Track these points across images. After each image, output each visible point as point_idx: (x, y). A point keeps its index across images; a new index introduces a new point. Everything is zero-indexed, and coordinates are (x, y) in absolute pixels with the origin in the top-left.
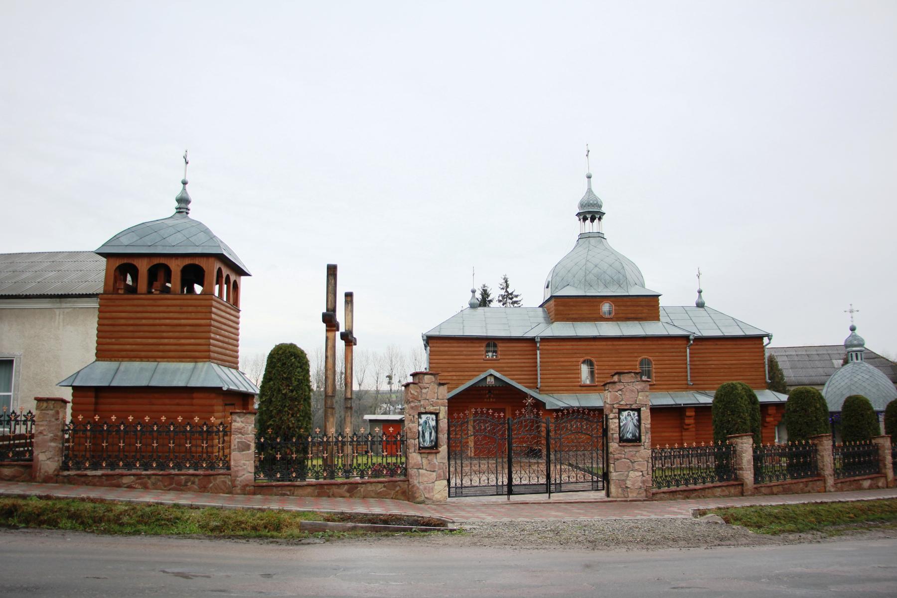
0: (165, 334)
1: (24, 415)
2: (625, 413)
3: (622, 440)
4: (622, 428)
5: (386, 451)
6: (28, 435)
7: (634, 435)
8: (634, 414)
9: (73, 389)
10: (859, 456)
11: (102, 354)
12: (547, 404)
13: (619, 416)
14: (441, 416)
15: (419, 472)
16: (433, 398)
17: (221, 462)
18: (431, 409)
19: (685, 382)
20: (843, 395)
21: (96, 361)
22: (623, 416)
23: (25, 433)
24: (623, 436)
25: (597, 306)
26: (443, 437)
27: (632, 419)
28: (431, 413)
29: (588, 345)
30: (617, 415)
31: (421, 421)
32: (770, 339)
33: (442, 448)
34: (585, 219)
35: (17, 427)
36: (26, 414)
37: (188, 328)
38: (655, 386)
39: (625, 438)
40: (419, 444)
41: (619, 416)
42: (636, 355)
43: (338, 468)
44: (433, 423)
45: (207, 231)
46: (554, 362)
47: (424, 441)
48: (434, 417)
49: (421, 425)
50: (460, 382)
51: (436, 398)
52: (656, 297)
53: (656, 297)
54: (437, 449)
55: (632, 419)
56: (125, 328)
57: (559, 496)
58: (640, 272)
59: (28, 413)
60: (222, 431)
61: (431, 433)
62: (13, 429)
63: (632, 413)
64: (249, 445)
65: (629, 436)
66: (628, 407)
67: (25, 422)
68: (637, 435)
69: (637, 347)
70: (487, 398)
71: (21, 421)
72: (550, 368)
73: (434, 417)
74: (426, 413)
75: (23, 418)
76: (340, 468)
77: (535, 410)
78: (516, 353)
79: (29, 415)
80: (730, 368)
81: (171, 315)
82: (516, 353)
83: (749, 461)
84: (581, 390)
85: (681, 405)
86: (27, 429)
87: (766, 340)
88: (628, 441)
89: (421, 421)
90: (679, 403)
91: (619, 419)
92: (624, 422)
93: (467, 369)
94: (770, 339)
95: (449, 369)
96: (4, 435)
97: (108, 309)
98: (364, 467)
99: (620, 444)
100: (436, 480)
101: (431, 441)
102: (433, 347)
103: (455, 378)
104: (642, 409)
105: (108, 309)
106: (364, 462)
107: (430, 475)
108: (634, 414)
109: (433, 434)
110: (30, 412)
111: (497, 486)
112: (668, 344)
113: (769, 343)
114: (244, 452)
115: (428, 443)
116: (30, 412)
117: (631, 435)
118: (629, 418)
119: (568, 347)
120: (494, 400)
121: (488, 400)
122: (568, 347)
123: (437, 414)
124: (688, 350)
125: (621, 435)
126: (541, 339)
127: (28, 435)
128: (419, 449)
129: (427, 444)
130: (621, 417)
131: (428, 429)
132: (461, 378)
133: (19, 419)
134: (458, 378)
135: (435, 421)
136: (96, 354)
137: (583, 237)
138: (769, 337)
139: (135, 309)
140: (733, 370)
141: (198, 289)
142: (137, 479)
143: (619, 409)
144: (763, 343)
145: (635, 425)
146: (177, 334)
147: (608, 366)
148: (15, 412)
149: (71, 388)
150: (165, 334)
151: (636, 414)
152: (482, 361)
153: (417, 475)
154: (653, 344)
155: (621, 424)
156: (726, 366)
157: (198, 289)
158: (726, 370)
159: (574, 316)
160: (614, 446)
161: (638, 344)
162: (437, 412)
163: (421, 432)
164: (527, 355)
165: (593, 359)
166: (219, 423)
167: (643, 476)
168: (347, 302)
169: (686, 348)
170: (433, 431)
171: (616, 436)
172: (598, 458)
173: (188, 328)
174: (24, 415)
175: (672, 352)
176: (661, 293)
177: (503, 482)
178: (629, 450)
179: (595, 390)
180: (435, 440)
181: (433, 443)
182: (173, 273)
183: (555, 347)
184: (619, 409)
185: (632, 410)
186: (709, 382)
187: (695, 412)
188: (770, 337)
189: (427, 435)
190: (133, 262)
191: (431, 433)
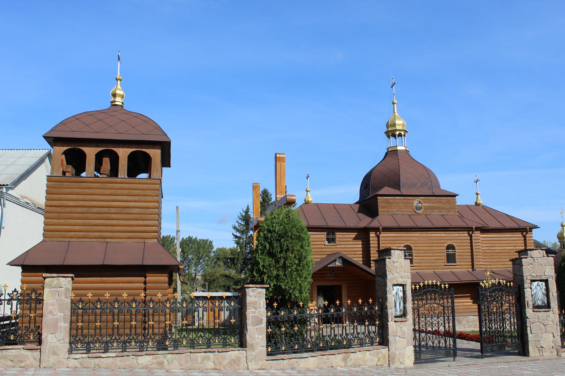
0: (113, 216)
1: (8, 294)
2: (535, 284)
4: (534, 296)
6: (13, 316)
7: (543, 302)
8: (542, 284)
9: (22, 269)
15: (395, 339)
16: (402, 272)
17: (201, 338)
20: (248, 296)
22: (533, 286)
23: (10, 314)
26: (409, 305)
27: (541, 289)
33: (409, 315)
37: (137, 210)
39: (536, 304)
42: (443, 241)
43: (30, 330)
44: (401, 294)
45: (159, 128)
48: (401, 288)
51: (403, 271)
55: (541, 289)
59: (13, 292)
60: (81, 309)
63: (540, 283)
64: (262, 320)
65: (539, 303)
68: (546, 302)
70: (328, 277)
71: (5, 300)
75: (8, 297)
79: (15, 293)
81: (119, 198)
86: (11, 309)
88: (539, 307)
92: (535, 291)
96: (4, 315)
97: (56, 190)
100: (407, 346)
101: (401, 311)
104: (549, 280)
105: (56, 190)
106: (362, 331)
108: (542, 284)
110: (15, 290)
116: (15, 290)
117: (541, 302)
118: (538, 288)
120: (333, 278)
121: (329, 279)
127: (13, 316)
130: (532, 286)
131: (398, 300)
135: (402, 293)
142: (152, 359)
145: (543, 294)
149: (20, 268)
150: (113, 216)
151: (544, 283)
152: (323, 246)
153: (394, 342)
156: (506, 251)
158: (506, 254)
160: (529, 312)
166: (166, 299)
167: (554, 337)
170: (401, 301)
171: (531, 303)
173: (137, 210)
174: (8, 294)
176: (458, 193)
178: (542, 314)
180: (403, 309)
181: (402, 312)
182: (120, 158)
185: (541, 281)
186: (495, 263)
190: (113, 149)
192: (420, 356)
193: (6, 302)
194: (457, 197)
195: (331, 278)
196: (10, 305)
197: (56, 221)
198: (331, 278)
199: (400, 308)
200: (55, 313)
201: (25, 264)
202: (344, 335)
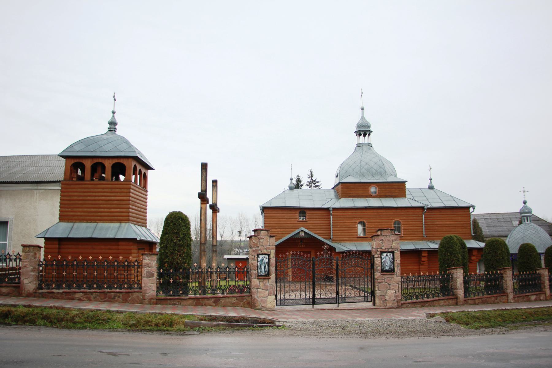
0: (101, 206)
1: (15, 256)
2: (385, 254)
3: (383, 271)
4: (383, 264)
5: (238, 278)
6: (17, 268)
7: (390, 268)
8: (390, 255)
9: (45, 239)
10: (529, 280)
11: (63, 218)
12: (336, 249)
13: (381, 256)
14: (271, 256)
15: (258, 290)
16: (267, 245)
17: (136, 284)
18: (265, 252)
19: (421, 235)
21: (59, 222)
22: (383, 256)
23: (15, 266)
24: (384, 268)
25: (367, 188)
26: (273, 269)
27: (389, 258)
28: (265, 254)
29: (362, 212)
30: (380, 255)
31: (259, 259)
32: (474, 209)
33: (272, 275)
34: (360, 135)
35: (11, 263)
36: (16, 255)
38: (403, 238)
39: (385, 269)
40: (258, 273)
41: (381, 256)
42: (391, 218)
44: (267, 261)
46: (341, 223)
47: (261, 272)
48: (267, 256)
49: (259, 261)
50: (283, 235)
51: (268, 245)
52: (404, 183)
53: (404, 183)
54: (269, 276)
55: (389, 258)
56: (77, 202)
57: (344, 305)
58: (394, 168)
59: (17, 254)
60: (136, 265)
61: (265, 267)
62: (8, 264)
63: (389, 254)
64: (153, 274)
65: (387, 268)
66: (387, 250)
67: (15, 260)
68: (392, 267)
69: (392, 213)
70: (300, 245)
71: (13, 259)
72: (338, 226)
73: (267, 256)
74: (262, 254)
75: (14, 257)
76: (209, 288)
77: (329, 253)
78: (317, 217)
79: (18, 255)
80: (449, 227)
81: (105, 194)
82: (317, 217)
83: (461, 284)
84: (358, 240)
85: (419, 249)
86: (16, 264)
87: (471, 209)
88: (386, 271)
89: (259, 259)
90: (418, 248)
91: (381, 258)
92: (384, 260)
93: (287, 227)
94: (474, 209)
95: (276, 227)
98: (224, 288)
99: (382, 273)
100: (268, 296)
101: (265, 272)
102: (267, 213)
103: (280, 232)
104: (395, 252)
107: (265, 292)
108: (390, 255)
109: (267, 267)
110: (18, 254)
111: (306, 299)
112: (411, 212)
113: (473, 211)
114: (150, 278)
115: (264, 273)
116: (18, 254)
117: (388, 268)
118: (387, 257)
119: (350, 214)
120: (304, 246)
122: (350, 214)
123: (269, 255)
124: (423, 216)
125: (382, 268)
126: (333, 208)
127: (17, 268)
128: (258, 277)
129: (263, 273)
130: (382, 256)
131: (263, 264)
132: (284, 232)
133: (12, 258)
134: (282, 232)
136: (59, 218)
137: (359, 146)
138: (473, 207)
139: (83, 190)
140: (451, 228)
141: (122, 178)
143: (381, 252)
144: (469, 211)
145: (391, 262)
146: (109, 206)
147: (374, 225)
148: (10, 253)
150: (101, 206)
151: (391, 255)
152: (297, 222)
153: (257, 292)
154: (402, 212)
155: (382, 261)
156: (447, 225)
157: (122, 178)
158: (447, 228)
159: (354, 195)
160: (378, 274)
161: (393, 212)
162: (269, 253)
163: (259, 266)
164: (324, 218)
165: (365, 221)
168: (213, 186)
169: (422, 214)
170: (266, 265)
171: (379, 268)
172: (368, 282)
173: (116, 202)
174: (15, 256)
175: (414, 217)
177: (309, 297)
178: (387, 277)
179: (366, 240)
180: (267, 271)
181: (267, 273)
183: (341, 214)
184: (381, 252)
185: (389, 252)
186: (436, 235)
187: (428, 253)
188: (474, 208)
189: (263, 268)
191: (265, 267)
192: (281, 303)
193: (3, 260)
194: (406, 183)
195: (302, 246)
196: (16, 262)
197: (67, 210)
198: (302, 246)
199: (265, 270)
200: (28, 267)
201: (46, 236)
202: (408, 293)
